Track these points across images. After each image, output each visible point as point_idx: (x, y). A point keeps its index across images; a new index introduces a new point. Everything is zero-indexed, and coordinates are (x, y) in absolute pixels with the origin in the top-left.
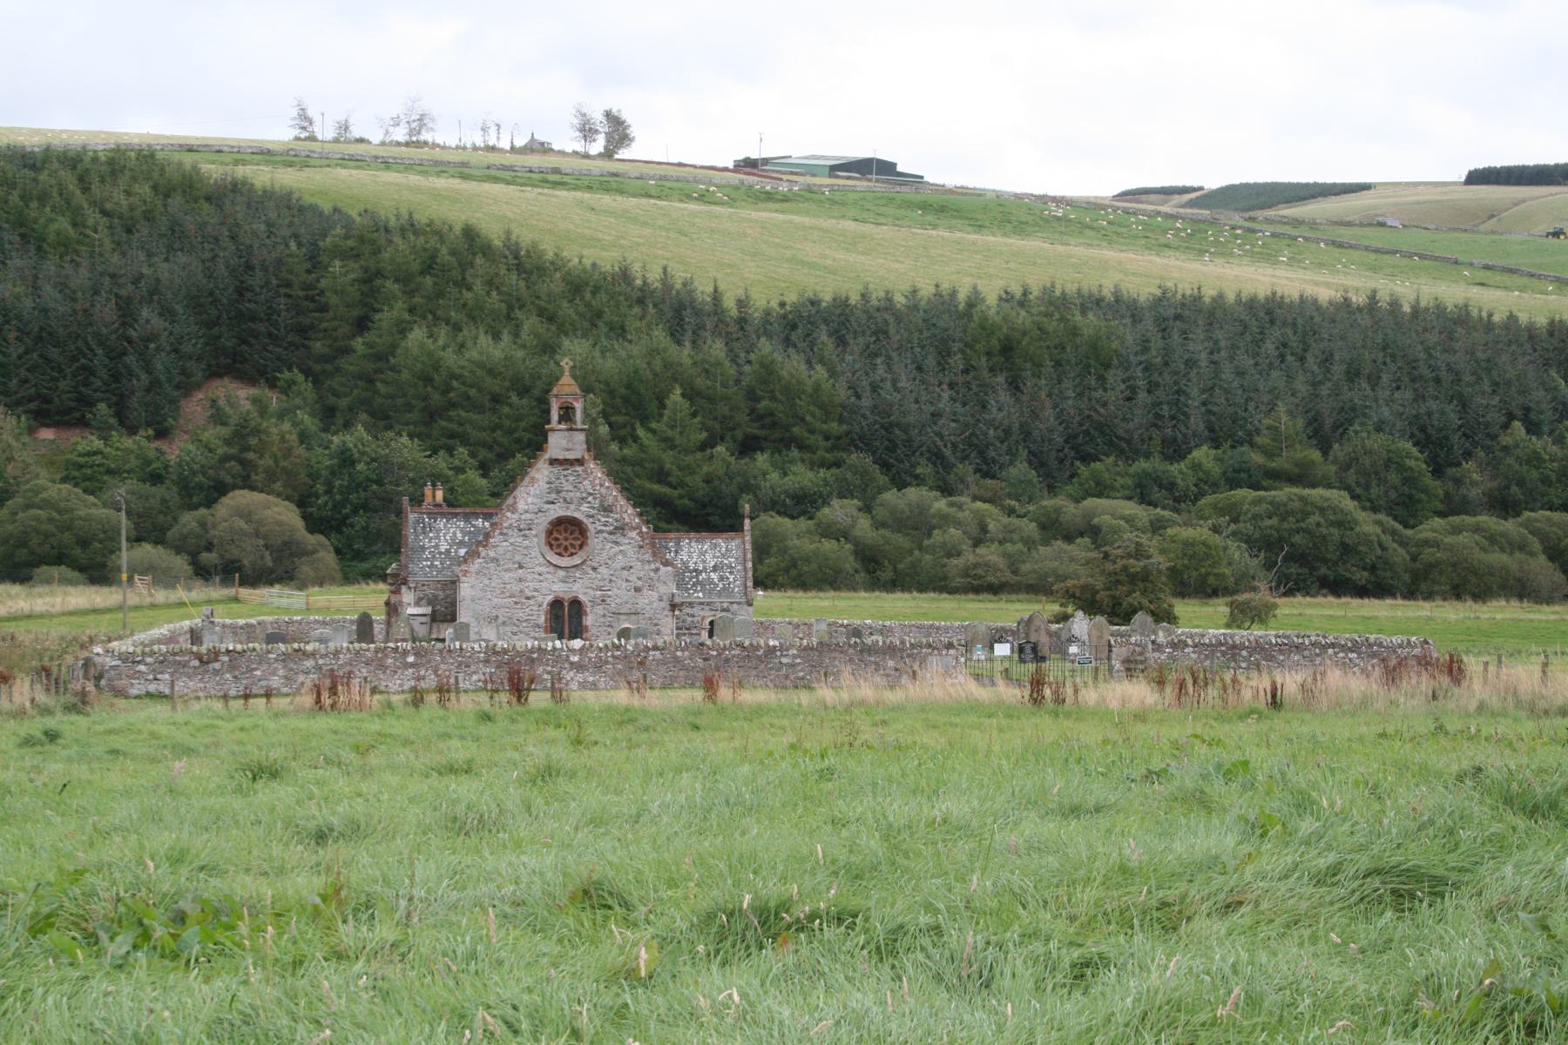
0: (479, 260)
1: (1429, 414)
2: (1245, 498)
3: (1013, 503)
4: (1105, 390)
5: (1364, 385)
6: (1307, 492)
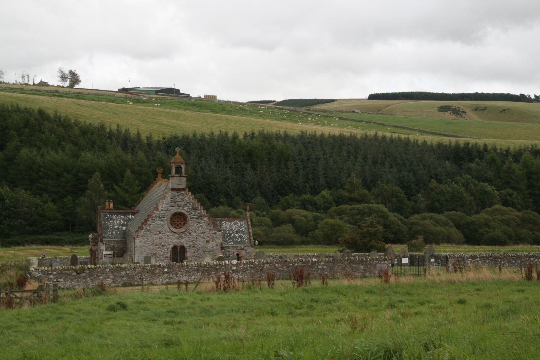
0: (46, 123)
1: (404, 177)
2: (347, 208)
3: (258, 211)
4: (288, 169)
5: (379, 166)
6: (370, 205)
